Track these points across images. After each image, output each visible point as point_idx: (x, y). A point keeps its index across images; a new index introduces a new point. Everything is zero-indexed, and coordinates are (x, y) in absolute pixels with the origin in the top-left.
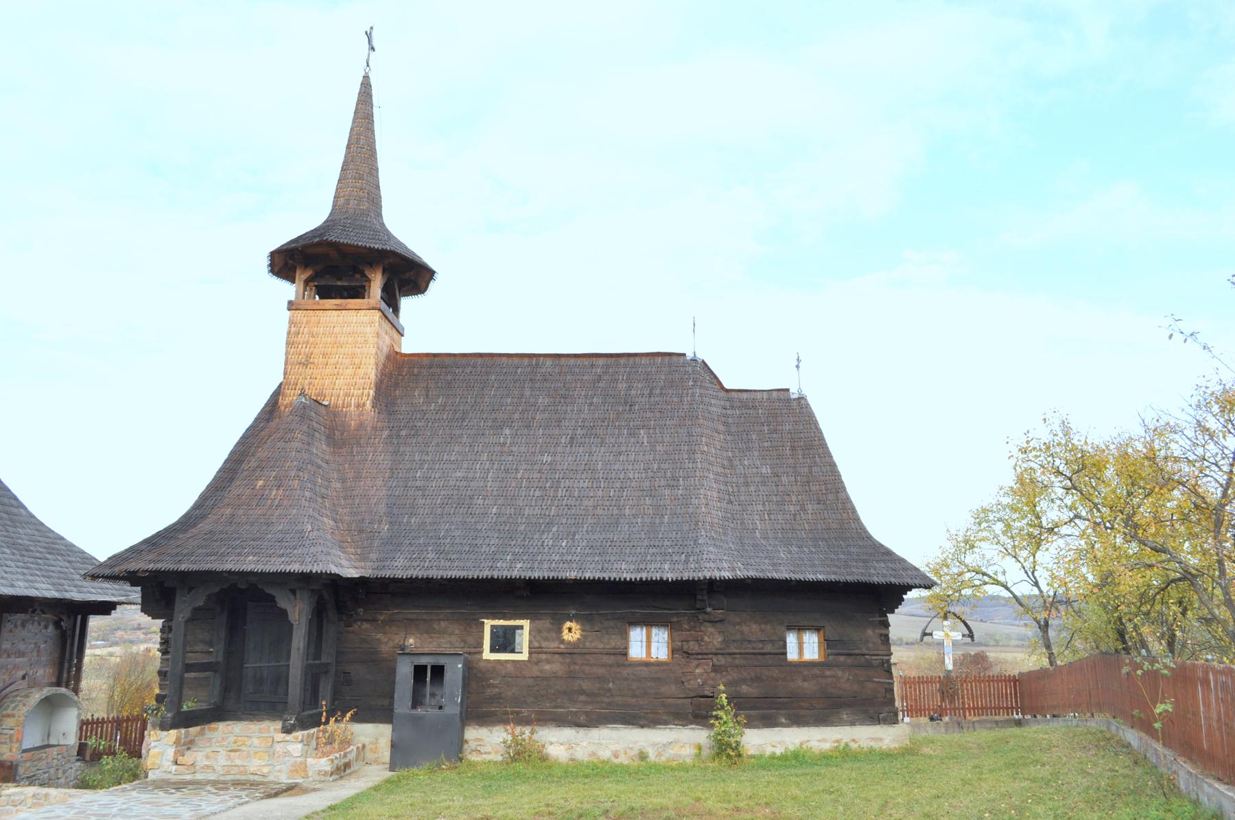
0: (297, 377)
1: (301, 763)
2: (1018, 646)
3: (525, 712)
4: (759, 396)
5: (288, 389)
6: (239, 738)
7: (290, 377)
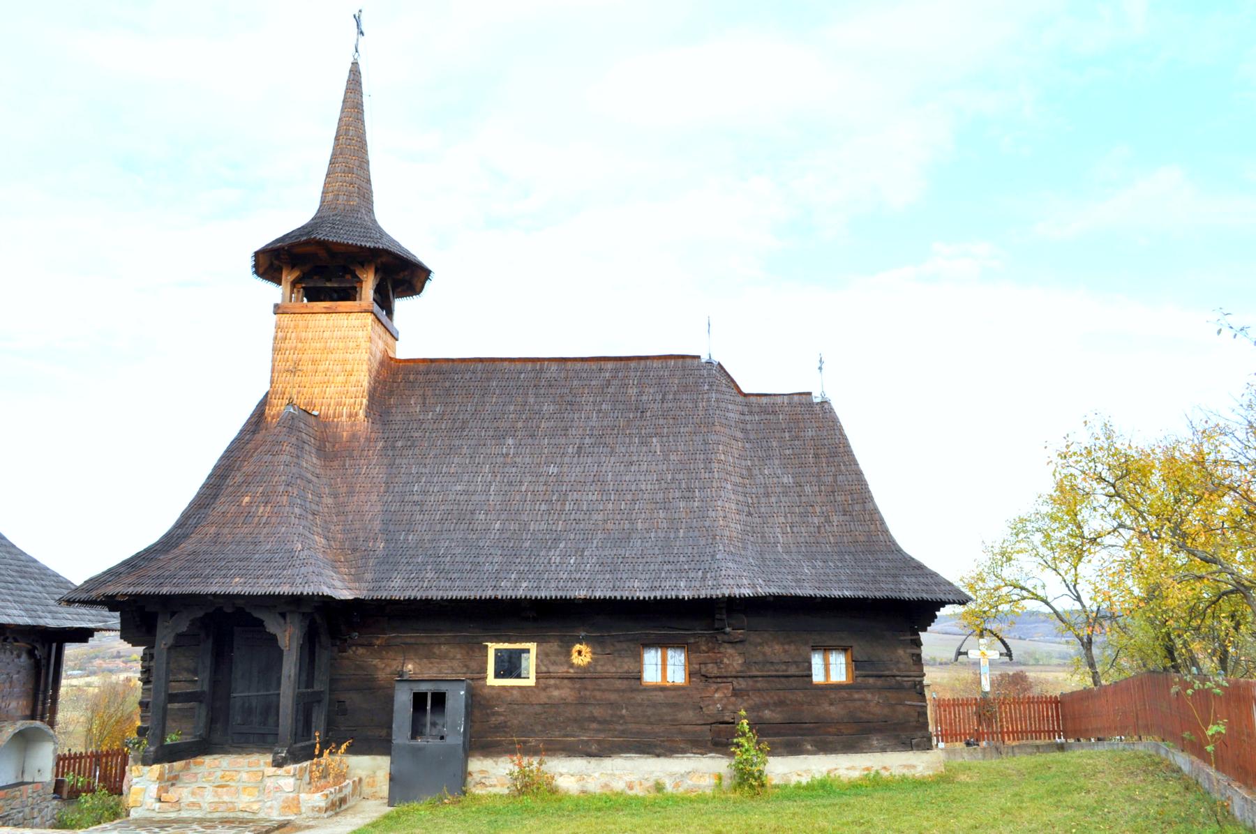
2: (1059, 665)
3: (532, 741)
4: (779, 400)
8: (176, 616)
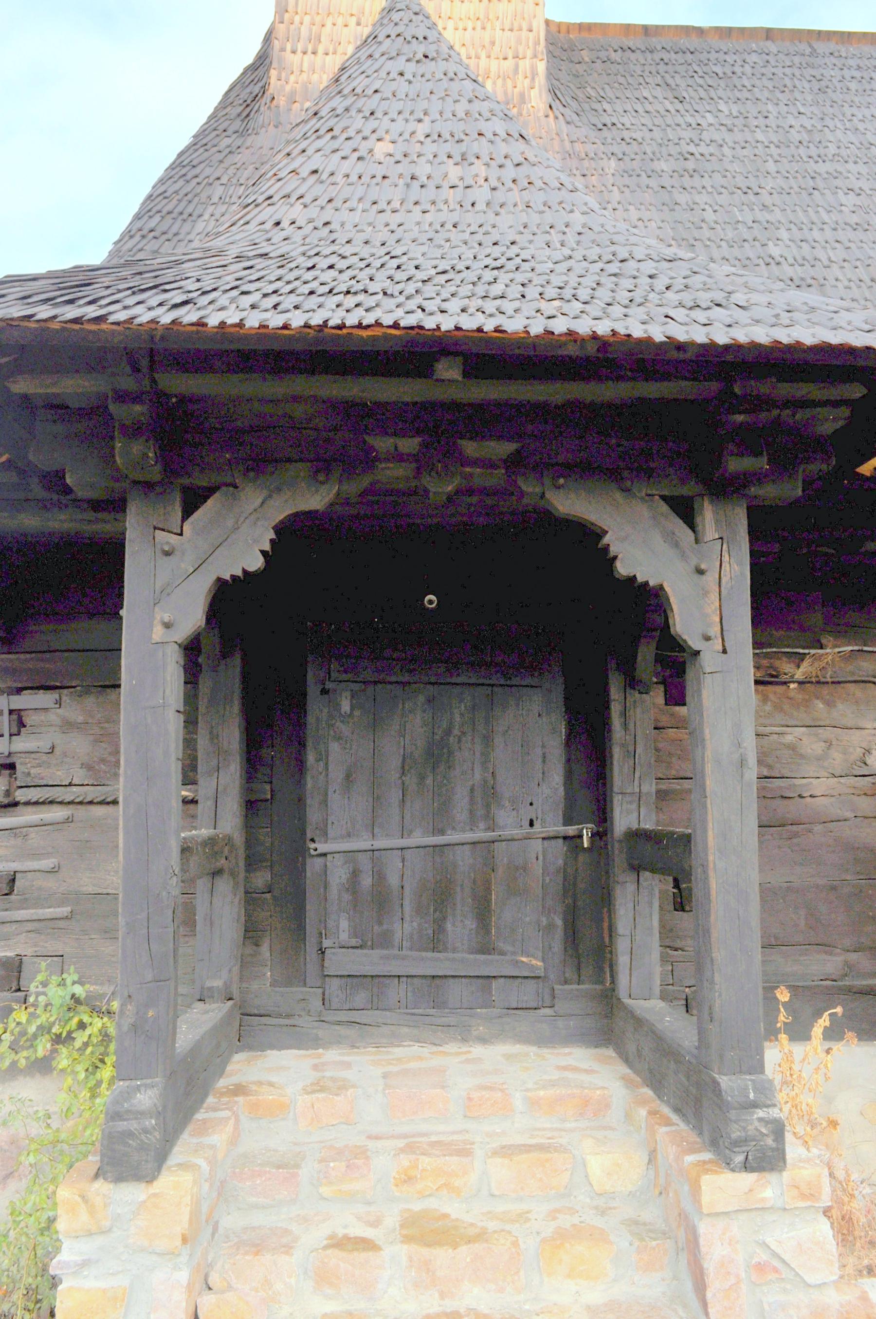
0: (318, 19)
5: (294, 52)
6: (425, 1162)
7: (297, 19)
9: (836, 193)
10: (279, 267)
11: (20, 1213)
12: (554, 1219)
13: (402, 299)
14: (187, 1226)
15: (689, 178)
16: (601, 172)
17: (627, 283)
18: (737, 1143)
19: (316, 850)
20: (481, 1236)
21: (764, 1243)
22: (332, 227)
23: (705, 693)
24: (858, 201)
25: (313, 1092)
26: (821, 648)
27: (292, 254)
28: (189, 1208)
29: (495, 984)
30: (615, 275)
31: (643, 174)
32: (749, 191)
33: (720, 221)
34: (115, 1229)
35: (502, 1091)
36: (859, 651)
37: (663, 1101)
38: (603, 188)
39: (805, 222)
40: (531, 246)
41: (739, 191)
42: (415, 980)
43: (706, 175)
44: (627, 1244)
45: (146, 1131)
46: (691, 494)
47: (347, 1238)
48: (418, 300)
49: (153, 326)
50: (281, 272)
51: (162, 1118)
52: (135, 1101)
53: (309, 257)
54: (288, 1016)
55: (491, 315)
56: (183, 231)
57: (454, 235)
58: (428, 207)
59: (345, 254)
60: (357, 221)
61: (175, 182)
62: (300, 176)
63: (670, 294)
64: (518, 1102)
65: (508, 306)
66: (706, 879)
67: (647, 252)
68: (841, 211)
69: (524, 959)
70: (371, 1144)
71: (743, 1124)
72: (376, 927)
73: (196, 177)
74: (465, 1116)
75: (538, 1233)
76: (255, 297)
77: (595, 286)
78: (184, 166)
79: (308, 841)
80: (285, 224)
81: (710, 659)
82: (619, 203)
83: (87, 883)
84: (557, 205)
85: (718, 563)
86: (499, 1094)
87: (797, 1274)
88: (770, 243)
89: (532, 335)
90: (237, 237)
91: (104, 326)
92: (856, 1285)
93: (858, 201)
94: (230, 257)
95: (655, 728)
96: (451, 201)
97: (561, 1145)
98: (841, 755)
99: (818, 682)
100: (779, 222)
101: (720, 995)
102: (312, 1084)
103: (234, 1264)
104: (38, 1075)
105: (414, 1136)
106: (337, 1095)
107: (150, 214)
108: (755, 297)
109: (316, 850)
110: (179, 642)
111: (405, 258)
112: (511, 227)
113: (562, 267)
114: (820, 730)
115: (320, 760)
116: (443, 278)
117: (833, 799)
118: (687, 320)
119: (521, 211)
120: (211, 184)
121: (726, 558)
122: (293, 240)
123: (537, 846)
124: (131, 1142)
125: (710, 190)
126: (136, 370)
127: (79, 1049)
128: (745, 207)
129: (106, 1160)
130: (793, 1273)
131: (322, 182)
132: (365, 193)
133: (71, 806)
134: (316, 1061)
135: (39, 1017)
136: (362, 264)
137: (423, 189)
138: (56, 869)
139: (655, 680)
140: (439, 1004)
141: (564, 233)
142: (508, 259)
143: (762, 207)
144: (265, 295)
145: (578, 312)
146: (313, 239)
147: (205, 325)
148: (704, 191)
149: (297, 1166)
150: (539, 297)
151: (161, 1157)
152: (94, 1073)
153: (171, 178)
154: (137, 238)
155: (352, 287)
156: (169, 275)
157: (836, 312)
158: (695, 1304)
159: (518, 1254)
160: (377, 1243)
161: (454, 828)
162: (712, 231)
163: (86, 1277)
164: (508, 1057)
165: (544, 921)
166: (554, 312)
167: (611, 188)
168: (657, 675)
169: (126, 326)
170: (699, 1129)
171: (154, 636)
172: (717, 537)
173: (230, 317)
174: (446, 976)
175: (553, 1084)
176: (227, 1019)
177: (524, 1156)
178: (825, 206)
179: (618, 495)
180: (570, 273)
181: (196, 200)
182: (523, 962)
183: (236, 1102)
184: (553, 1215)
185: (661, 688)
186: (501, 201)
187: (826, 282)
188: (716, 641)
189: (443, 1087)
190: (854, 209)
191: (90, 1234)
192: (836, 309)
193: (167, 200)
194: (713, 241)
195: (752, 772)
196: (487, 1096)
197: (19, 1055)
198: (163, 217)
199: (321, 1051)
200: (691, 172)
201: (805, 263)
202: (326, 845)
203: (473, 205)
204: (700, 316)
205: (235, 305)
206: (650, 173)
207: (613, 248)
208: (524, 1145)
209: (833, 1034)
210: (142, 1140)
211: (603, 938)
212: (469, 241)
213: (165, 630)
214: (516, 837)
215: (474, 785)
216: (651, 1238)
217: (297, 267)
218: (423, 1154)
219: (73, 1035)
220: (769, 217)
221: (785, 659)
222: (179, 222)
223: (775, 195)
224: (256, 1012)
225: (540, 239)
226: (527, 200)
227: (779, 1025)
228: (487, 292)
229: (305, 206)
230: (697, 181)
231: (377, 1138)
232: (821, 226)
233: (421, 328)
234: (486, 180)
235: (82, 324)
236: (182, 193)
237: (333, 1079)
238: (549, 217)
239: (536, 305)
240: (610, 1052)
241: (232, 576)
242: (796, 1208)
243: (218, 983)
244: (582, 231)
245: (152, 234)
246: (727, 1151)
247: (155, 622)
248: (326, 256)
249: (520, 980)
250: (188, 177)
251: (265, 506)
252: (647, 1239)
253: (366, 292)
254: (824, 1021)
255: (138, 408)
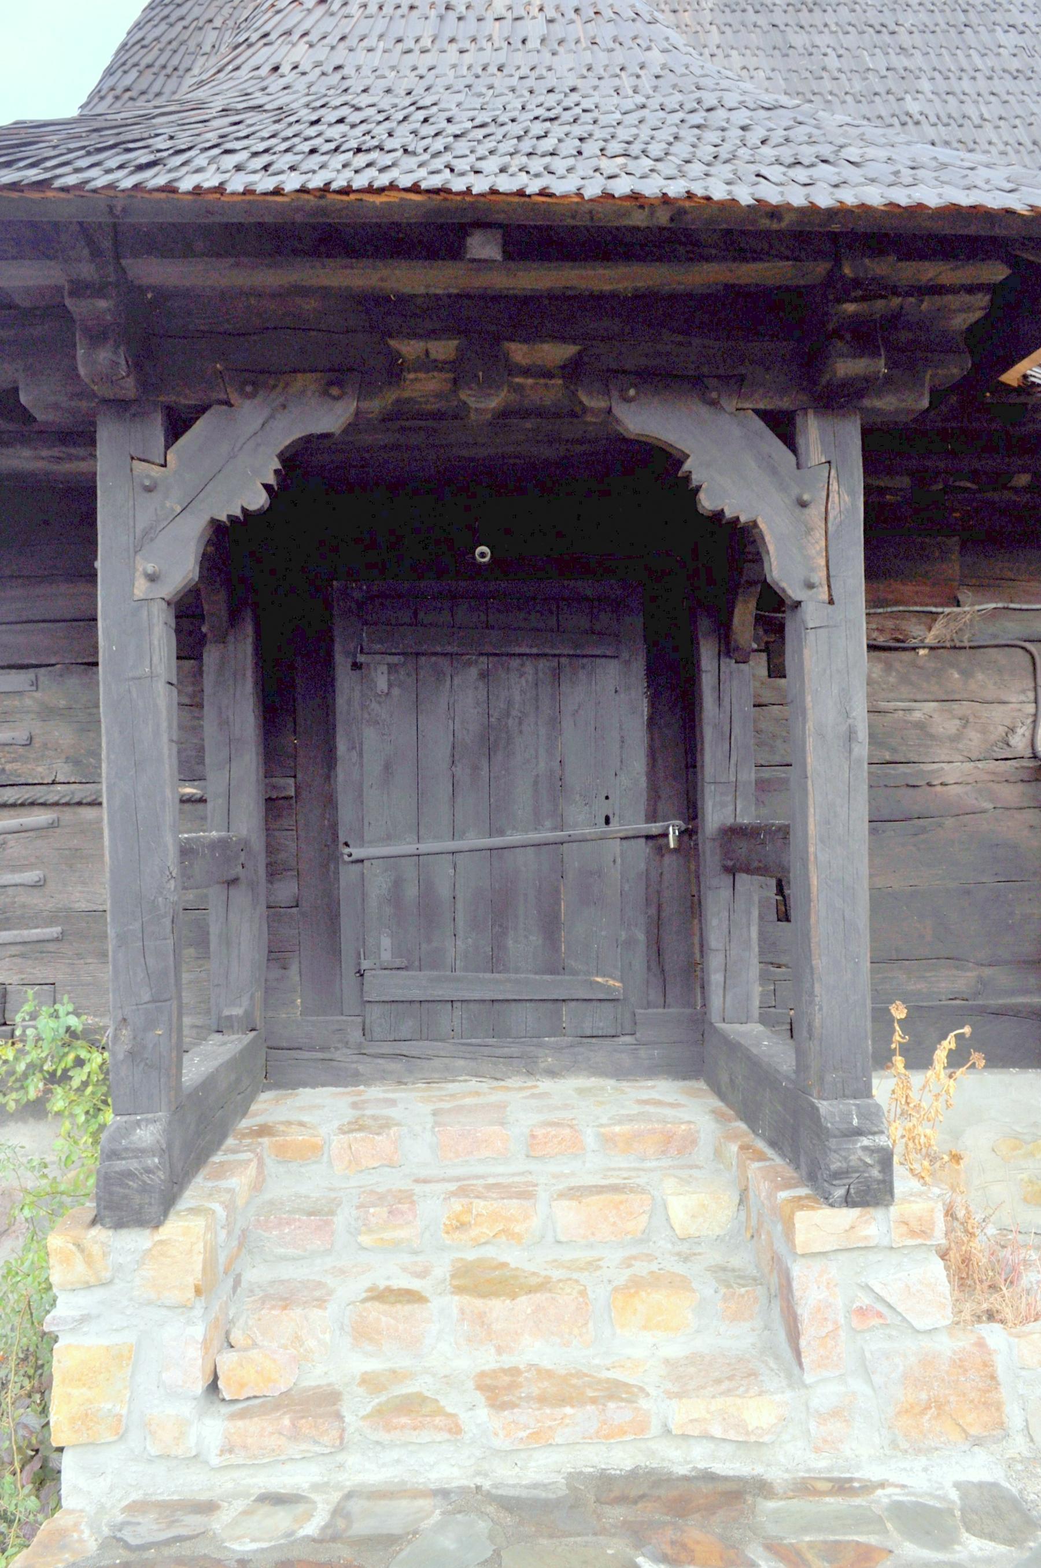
1: (960, 1364)
6: (480, 1206)
8: (199, 426)
9: (993, 31)
10: (275, 122)
11: (17, 1273)
12: (629, 1266)
13: (426, 156)
14: (200, 1277)
15: (807, 14)
16: (697, 7)
17: (713, 137)
18: (837, 1175)
19: (350, 855)
20: (544, 1286)
21: (867, 1286)
22: (345, 72)
23: (806, 652)
24: (1020, 41)
25: (351, 1131)
26: (958, 605)
27: (293, 106)
28: (201, 1257)
29: (564, 1008)
30: (698, 127)
31: (749, 8)
32: (884, 29)
33: (846, 68)
34: (116, 1281)
35: (571, 1127)
36: (1004, 608)
37: (758, 1135)
38: (699, 28)
39: (953, 69)
40: (596, 93)
41: (871, 30)
42: (472, 1006)
43: (829, 9)
44: (712, 1291)
45: (148, 1171)
46: (792, 408)
47: (389, 1290)
48: (447, 157)
49: (111, 193)
50: (277, 127)
51: (166, 1156)
52: (135, 1138)
53: (314, 109)
54: (322, 1049)
55: (537, 175)
56: (167, 90)
57: (501, 82)
58: (466, 44)
59: (358, 105)
60: (376, 63)
61: (155, 26)
62: (305, 7)
63: (765, 150)
64: (589, 1138)
65: (559, 165)
66: (807, 877)
67: (742, 98)
68: (999, 54)
69: (599, 979)
70: (418, 1189)
71: (843, 1154)
72: (424, 946)
73: (182, 18)
74: (528, 1156)
75: (610, 1281)
76: (243, 156)
77: (672, 140)
78: (166, 5)
79: (341, 845)
80: (285, 69)
81: (813, 612)
82: (718, 47)
83: (79, 899)
84: (630, 41)
85: (824, 494)
86: (567, 1131)
87: (904, 1319)
88: (908, 97)
89: (586, 198)
90: (225, 86)
91: (50, 194)
92: (972, 1331)
93: (1020, 41)
94: (214, 111)
95: (755, 706)
96: (495, 37)
97: (639, 1186)
98: (979, 735)
99: (955, 648)
100: (920, 69)
101: (821, 1009)
102: (349, 1123)
103: (259, 1320)
104: (31, 1120)
105: (468, 1178)
106: (378, 1134)
107: (125, 68)
108: (871, 152)
109: (350, 855)
110: (167, 598)
111: (435, 109)
112: (571, 70)
113: (633, 118)
114: (955, 706)
115: (354, 748)
116: (480, 133)
117: (969, 787)
118: (783, 179)
119: (585, 49)
120: (200, 29)
121: (834, 486)
122: (294, 89)
123: (616, 846)
124: (131, 1183)
125: (834, 28)
126: (96, 253)
127: (78, 1090)
128: (877, 50)
129: (103, 1203)
130: (900, 1318)
131: (332, 14)
132: (388, 27)
133: (56, 808)
134: (356, 1099)
135: (28, 1053)
136: (381, 117)
137: (462, 23)
138: (41, 883)
139: (755, 646)
140: (499, 1032)
141: (638, 76)
142: (565, 109)
143: (898, 50)
144: (255, 154)
145: (647, 170)
146: (320, 88)
147: (175, 191)
148: (826, 30)
149: (332, 1213)
150: (599, 153)
151: (168, 1201)
152: (95, 1116)
153: (149, 21)
154: (109, 99)
155: (364, 143)
156: (136, 132)
157: (972, 169)
158: (788, 1354)
159: (587, 1304)
160: (423, 1294)
161: (514, 828)
162: (834, 82)
163: (85, 1334)
164: (580, 1091)
165: (623, 935)
166: (617, 171)
167: (708, 27)
168: (756, 639)
169: (78, 193)
170: (795, 1162)
171: (136, 591)
172: (823, 460)
173: (208, 180)
174: (507, 1001)
175: (630, 1118)
176: (247, 1054)
177: (597, 1197)
178: (980, 48)
179: (704, 411)
180: (641, 126)
181: (183, 48)
182: (598, 982)
183: (260, 1144)
184: (628, 1262)
185: (764, 655)
186: (560, 36)
187: (976, 146)
188: (820, 589)
189: (502, 1124)
190: (1015, 51)
191: (88, 1286)
192: (973, 165)
193: (145, 50)
194: (836, 95)
195: (862, 750)
196: (554, 1132)
197: (7, 1098)
198: (141, 72)
199: (362, 1088)
200: (811, 5)
201: (952, 121)
202: (362, 850)
203: (524, 42)
204: (801, 174)
205: (214, 167)
206: (758, 7)
207: (698, 94)
208: (595, 1186)
209: (957, 1059)
210: (144, 1182)
211: (693, 953)
212: (518, 88)
213: (148, 584)
214: (589, 838)
215: (538, 776)
216: (739, 1284)
217: (297, 121)
218: (478, 1197)
219: (70, 1074)
220: (906, 62)
221: (914, 620)
222: (161, 79)
223: (916, 35)
224: (285, 1045)
225: (607, 85)
226: (592, 34)
227: (893, 1046)
228: (534, 147)
229: (311, 46)
230: (817, 17)
231: (425, 1181)
232: (972, 73)
233: (449, 191)
234: (541, 10)
235: (22, 191)
236: (164, 40)
237: (374, 1118)
238: (620, 56)
239: (594, 162)
240: (702, 1085)
241: (229, 516)
242: (904, 1247)
243: (237, 1011)
244: (661, 73)
245: (128, 94)
246: (826, 1185)
247: (137, 574)
248: (336, 108)
249: (595, 1004)
250: (172, 19)
251: (267, 427)
252: (735, 1286)
253: (382, 149)
254: (949, 1043)
255: (102, 304)
